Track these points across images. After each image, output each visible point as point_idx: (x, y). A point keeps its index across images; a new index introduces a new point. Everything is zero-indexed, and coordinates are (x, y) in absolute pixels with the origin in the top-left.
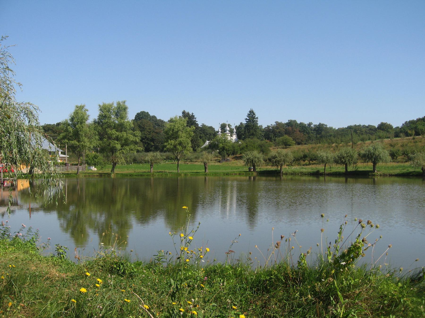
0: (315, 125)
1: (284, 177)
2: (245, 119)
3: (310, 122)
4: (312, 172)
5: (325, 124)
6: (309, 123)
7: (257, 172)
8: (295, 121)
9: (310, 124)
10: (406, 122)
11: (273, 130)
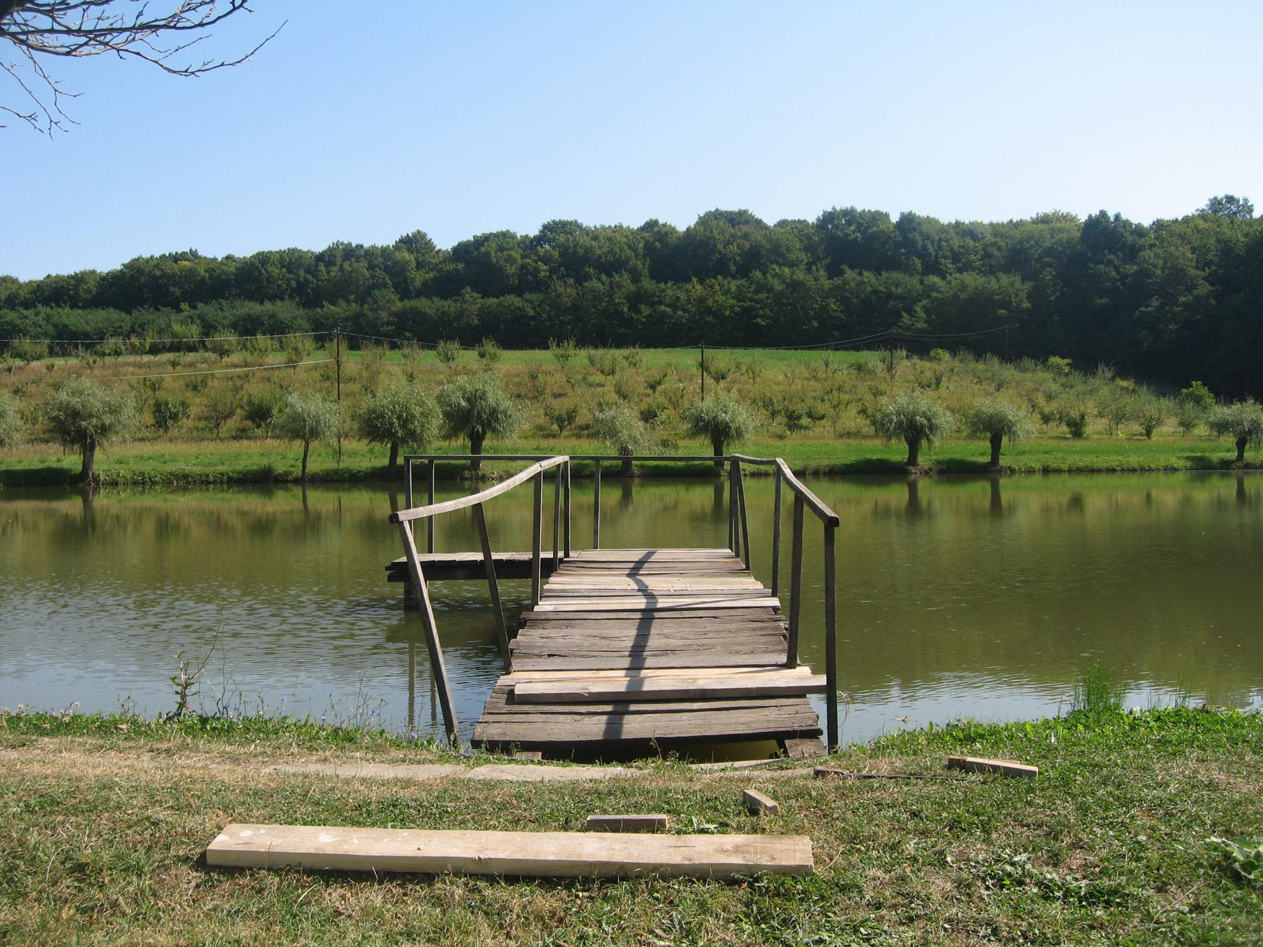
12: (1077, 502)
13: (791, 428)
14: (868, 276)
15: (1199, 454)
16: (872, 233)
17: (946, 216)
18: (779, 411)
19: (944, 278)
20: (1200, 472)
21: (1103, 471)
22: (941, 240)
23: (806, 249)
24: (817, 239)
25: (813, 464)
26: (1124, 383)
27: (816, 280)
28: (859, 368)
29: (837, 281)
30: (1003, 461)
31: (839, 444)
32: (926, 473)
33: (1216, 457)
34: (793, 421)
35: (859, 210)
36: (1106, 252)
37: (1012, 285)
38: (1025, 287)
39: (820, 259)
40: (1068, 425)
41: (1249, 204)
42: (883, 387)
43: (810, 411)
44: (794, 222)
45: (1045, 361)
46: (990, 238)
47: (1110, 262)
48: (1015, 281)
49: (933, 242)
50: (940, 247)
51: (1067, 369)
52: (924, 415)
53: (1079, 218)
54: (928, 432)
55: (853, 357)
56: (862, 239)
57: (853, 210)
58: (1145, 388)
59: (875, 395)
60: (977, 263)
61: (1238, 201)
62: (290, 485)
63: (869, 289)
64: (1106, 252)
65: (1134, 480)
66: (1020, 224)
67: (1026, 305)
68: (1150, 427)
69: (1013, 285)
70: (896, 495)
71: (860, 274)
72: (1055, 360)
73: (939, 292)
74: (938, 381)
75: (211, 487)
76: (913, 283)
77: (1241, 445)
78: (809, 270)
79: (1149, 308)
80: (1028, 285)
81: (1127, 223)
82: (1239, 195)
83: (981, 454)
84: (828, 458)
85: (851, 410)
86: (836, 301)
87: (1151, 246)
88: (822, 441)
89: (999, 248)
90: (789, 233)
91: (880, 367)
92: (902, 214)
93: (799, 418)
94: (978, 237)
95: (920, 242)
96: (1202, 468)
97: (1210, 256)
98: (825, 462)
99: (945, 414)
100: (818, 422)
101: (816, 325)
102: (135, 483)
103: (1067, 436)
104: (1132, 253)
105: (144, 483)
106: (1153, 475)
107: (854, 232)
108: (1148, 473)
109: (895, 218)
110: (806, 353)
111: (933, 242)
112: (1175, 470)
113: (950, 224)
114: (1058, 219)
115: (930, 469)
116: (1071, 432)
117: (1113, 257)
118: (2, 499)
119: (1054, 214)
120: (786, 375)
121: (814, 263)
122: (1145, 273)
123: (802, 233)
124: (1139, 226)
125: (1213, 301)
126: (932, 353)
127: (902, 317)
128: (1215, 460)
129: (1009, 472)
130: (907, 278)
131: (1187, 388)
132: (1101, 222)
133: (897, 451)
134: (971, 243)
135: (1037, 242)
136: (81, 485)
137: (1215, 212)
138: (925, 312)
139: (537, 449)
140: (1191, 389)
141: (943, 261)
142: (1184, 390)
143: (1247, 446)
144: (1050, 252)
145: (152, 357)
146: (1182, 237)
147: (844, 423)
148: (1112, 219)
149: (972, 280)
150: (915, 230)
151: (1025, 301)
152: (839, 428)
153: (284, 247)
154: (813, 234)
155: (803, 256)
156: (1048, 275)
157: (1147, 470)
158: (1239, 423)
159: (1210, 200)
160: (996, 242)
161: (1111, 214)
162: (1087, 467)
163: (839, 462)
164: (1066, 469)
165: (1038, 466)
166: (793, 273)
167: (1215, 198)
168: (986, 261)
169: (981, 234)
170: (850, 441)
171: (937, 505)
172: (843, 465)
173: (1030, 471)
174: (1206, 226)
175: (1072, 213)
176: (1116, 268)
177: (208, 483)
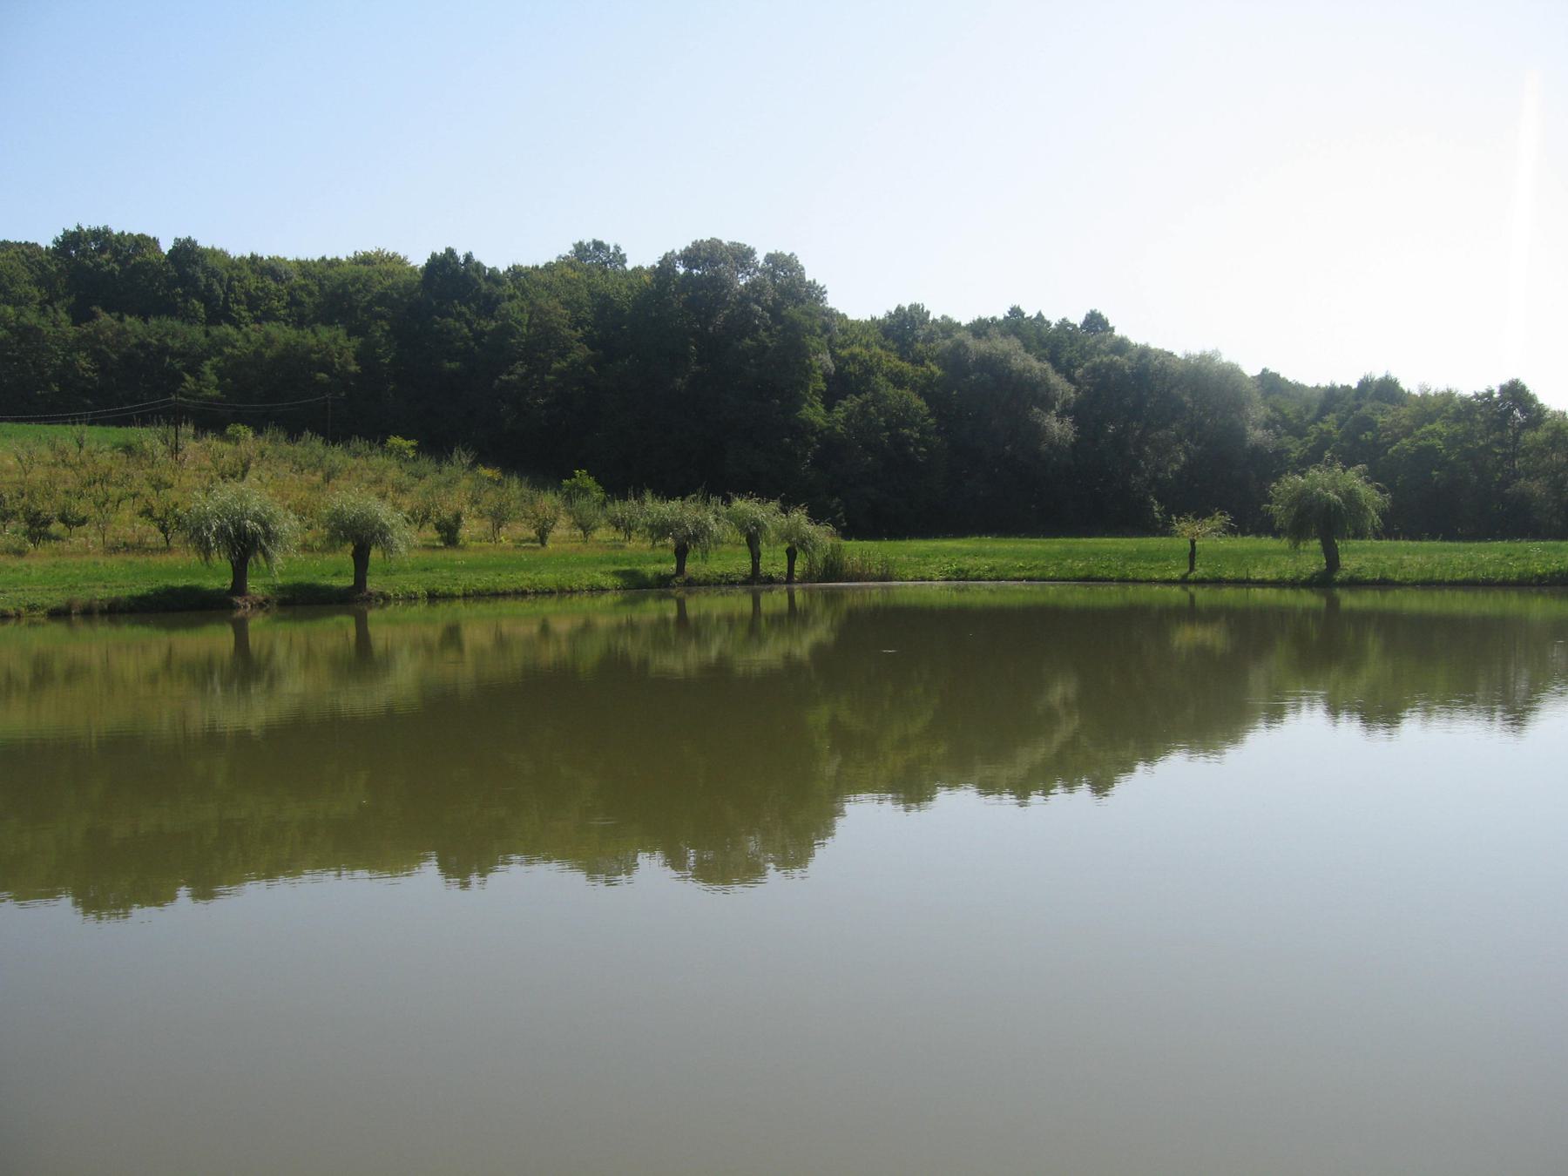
12: (452, 635)
13: (34, 538)
14: (132, 323)
15: (627, 568)
16: (134, 265)
17: (238, 248)
18: (14, 513)
19: (238, 328)
20: (633, 592)
21: (509, 594)
22: (231, 279)
23: (39, 283)
24: (54, 269)
25: (81, 597)
26: (487, 472)
27: (54, 325)
28: (128, 449)
29: (87, 328)
30: (373, 584)
31: (114, 561)
32: (261, 605)
33: (650, 570)
34: (37, 528)
35: (115, 233)
36: (456, 302)
37: (335, 340)
38: (351, 344)
39: (58, 298)
40: (438, 528)
41: (621, 253)
42: (167, 476)
43: (64, 514)
44: (19, 244)
45: (383, 442)
46: (297, 279)
47: (461, 315)
48: (338, 336)
49: (221, 281)
50: (230, 289)
51: (411, 454)
52: (257, 518)
53: (408, 260)
54: (263, 542)
55: (118, 434)
56: (120, 272)
57: (107, 231)
58: (516, 480)
59: (156, 488)
60: (282, 312)
61: (608, 248)
63: (133, 341)
64: (456, 302)
65: (523, 607)
66: (336, 262)
67: (353, 368)
68: (545, 530)
69: (332, 339)
70: (216, 640)
71: (121, 319)
72: (395, 441)
73: (234, 347)
74: (246, 468)
76: (197, 332)
77: (681, 553)
78: (43, 311)
79: (512, 377)
80: (356, 341)
81: (479, 267)
82: (610, 241)
83: (336, 575)
84: (105, 587)
85: (123, 509)
86: (87, 356)
87: (511, 298)
88: (85, 558)
89: (311, 294)
90: (13, 258)
91: (160, 448)
92: (177, 240)
93: (48, 522)
94: (281, 277)
95: (204, 280)
96: (636, 585)
97: (582, 314)
98: (102, 594)
99: (286, 516)
100: (75, 529)
101: (57, 389)
103: (437, 544)
104: (489, 305)
106: (576, 598)
107: (108, 262)
108: (568, 596)
109: (166, 247)
110: (47, 428)
111: (221, 281)
112: (603, 590)
113: (242, 259)
114: (383, 260)
115: (267, 600)
116: (442, 539)
117: (464, 309)
118: (7, 427)
119: (377, 254)
120: (19, 459)
121: (50, 302)
122: (506, 331)
123: (32, 260)
124: (494, 271)
125: (592, 369)
126: (229, 430)
127: (184, 380)
128: (650, 575)
129: (382, 601)
130: (185, 327)
131: (569, 478)
132: (449, 263)
133: (218, 577)
134: (273, 286)
135: (364, 285)
137: (580, 259)
138: (215, 374)
140: (573, 480)
141: (236, 307)
142: (566, 482)
143: (690, 555)
144: (382, 298)
145: (170, 583)
146: (548, 287)
147: (115, 530)
148: (462, 260)
149: (282, 333)
150: (196, 263)
151: (353, 362)
152: (110, 538)
154: (48, 262)
155: (34, 291)
156: (379, 330)
157: (568, 592)
158: (680, 525)
159: (575, 245)
160: (307, 285)
161: (461, 254)
162: (488, 590)
163: (125, 593)
164: (461, 593)
165: (421, 590)
166: (22, 314)
167: (581, 243)
168: (294, 309)
169: (285, 273)
170: (130, 558)
171: (281, 652)
172: (132, 597)
173: (411, 598)
174: (575, 275)
175: (399, 254)
176: (469, 323)
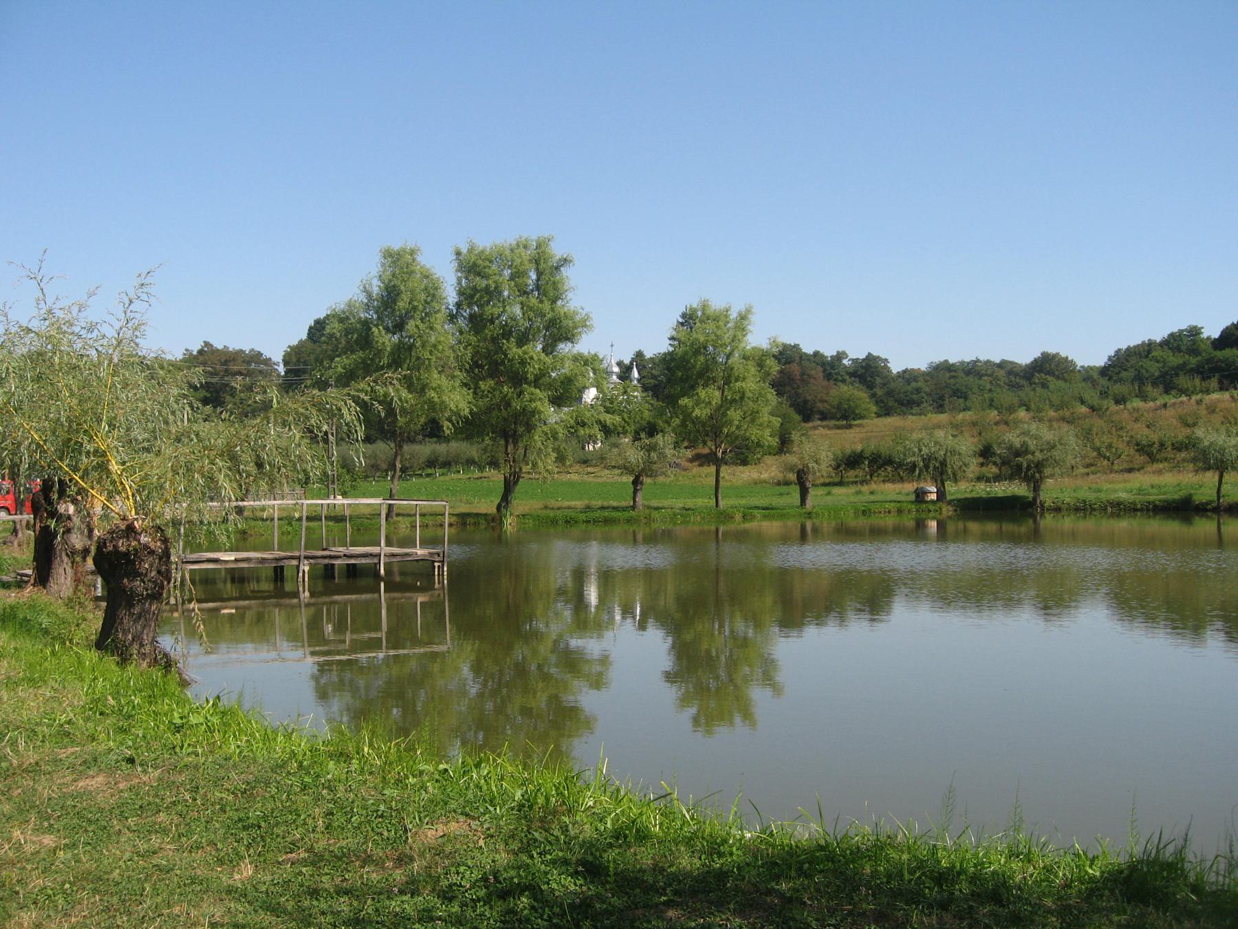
0: (855, 361)
1: (1047, 521)
2: (670, 339)
3: (840, 350)
4: (1160, 501)
5: (883, 357)
6: (838, 352)
7: (950, 503)
8: (796, 347)
9: (840, 356)
10: (1119, 350)
11: (832, 362)
62: (1209, 514)
75: (1139, 513)
98: (1155, 497)
102: (1077, 509)
105: (1084, 509)
136: (1030, 510)
139: (900, 493)
153: (968, 358)
177: (1136, 510)
